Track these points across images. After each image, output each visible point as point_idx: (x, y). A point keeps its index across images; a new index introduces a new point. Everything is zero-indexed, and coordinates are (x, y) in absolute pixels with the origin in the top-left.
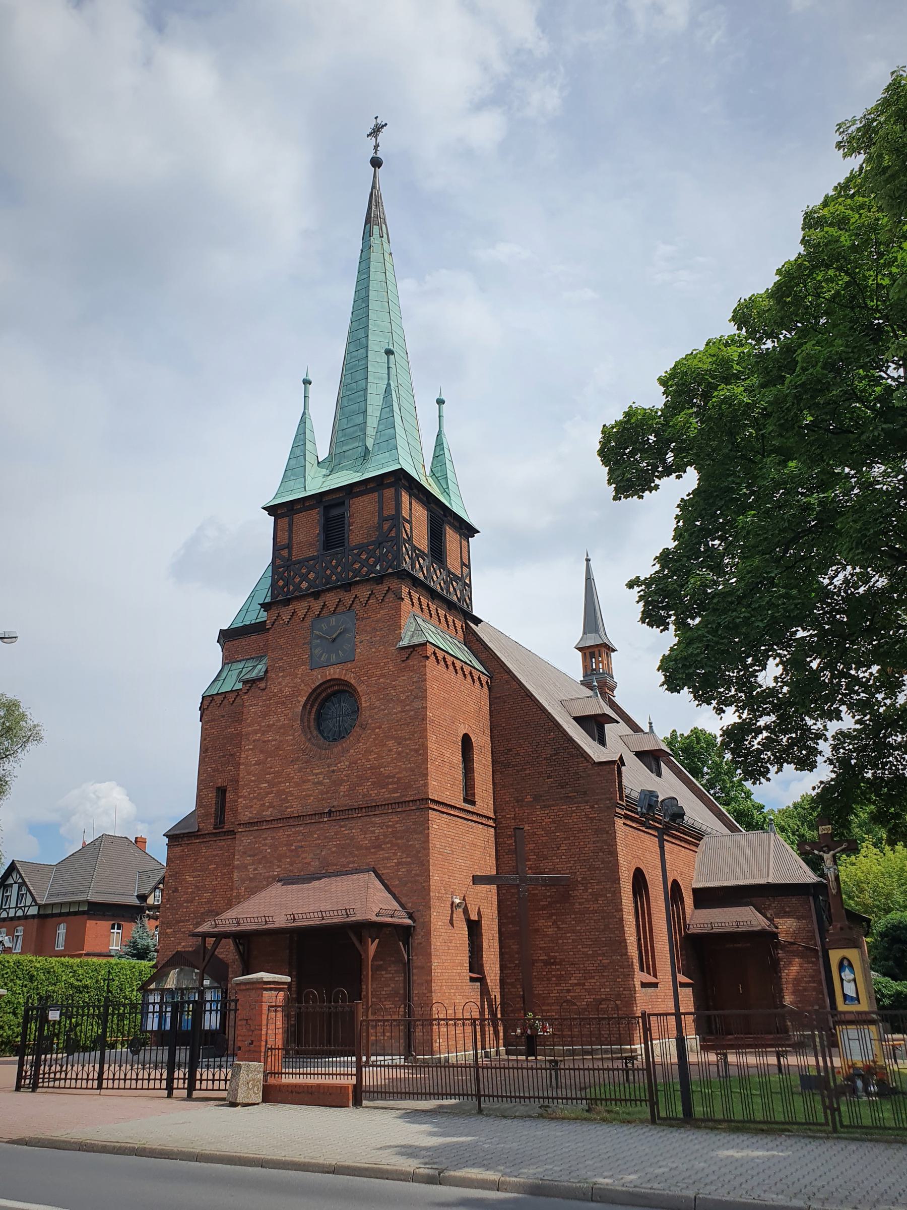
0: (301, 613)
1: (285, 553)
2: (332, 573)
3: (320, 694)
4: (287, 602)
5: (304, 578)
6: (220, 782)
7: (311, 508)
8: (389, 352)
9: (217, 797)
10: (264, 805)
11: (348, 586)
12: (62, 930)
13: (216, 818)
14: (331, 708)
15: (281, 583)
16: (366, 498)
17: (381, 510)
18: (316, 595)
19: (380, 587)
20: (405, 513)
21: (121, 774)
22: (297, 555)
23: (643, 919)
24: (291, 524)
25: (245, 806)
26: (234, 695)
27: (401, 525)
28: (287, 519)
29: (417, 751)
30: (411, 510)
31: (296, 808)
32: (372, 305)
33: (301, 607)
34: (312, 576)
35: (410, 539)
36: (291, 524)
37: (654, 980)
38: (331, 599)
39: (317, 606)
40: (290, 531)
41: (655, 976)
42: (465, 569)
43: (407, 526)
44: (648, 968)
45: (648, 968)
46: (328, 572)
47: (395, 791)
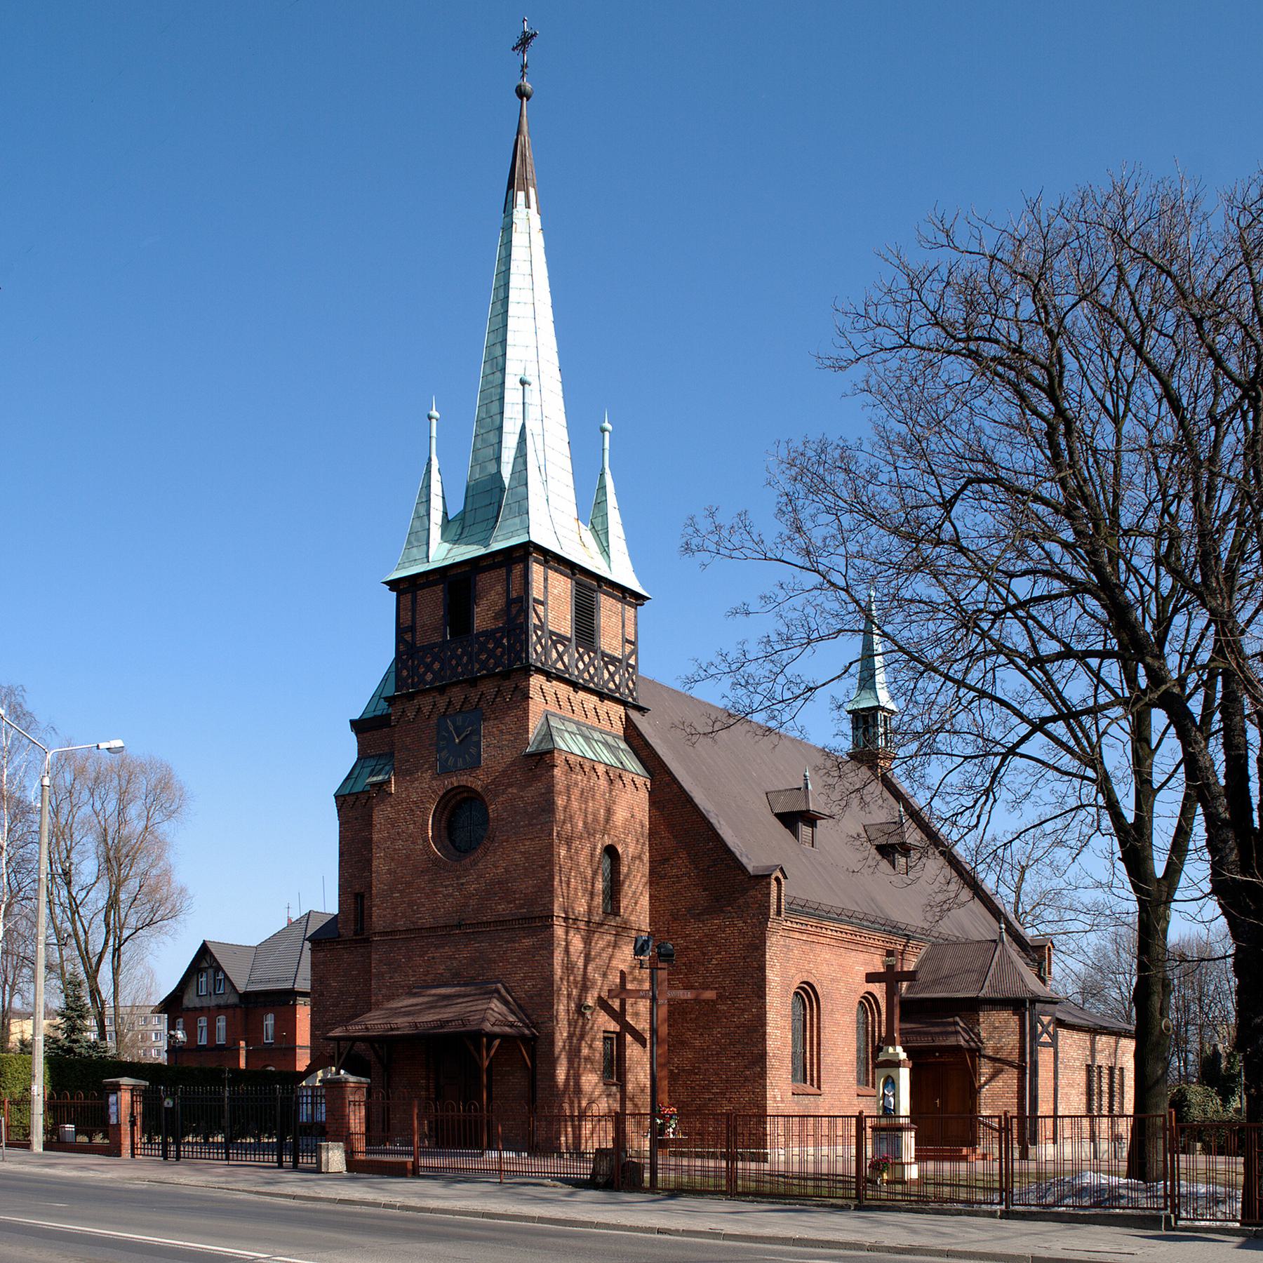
0: (426, 710)
1: (408, 637)
2: (458, 665)
3: (449, 801)
4: (410, 697)
5: (429, 668)
6: (357, 889)
7: (435, 583)
8: (523, 383)
9: (356, 903)
10: (396, 915)
11: (473, 682)
12: (269, 1021)
13: (356, 924)
14: (463, 818)
15: (405, 673)
16: (494, 574)
17: (508, 591)
18: (442, 690)
19: (507, 683)
20: (536, 592)
21: (254, 871)
22: (420, 641)
23: (812, 1031)
24: (414, 601)
25: (379, 917)
26: (353, 798)
27: (531, 610)
28: (409, 596)
29: (542, 867)
30: (545, 587)
31: (427, 920)
32: (513, 309)
33: (426, 703)
34: (437, 666)
35: (542, 627)
36: (414, 601)
37: (818, 1092)
38: (457, 695)
39: (442, 702)
40: (414, 611)
41: (819, 1088)
42: (629, 648)
43: (540, 609)
44: (812, 1080)
45: (812, 1080)
46: (454, 662)
47: (522, 906)
